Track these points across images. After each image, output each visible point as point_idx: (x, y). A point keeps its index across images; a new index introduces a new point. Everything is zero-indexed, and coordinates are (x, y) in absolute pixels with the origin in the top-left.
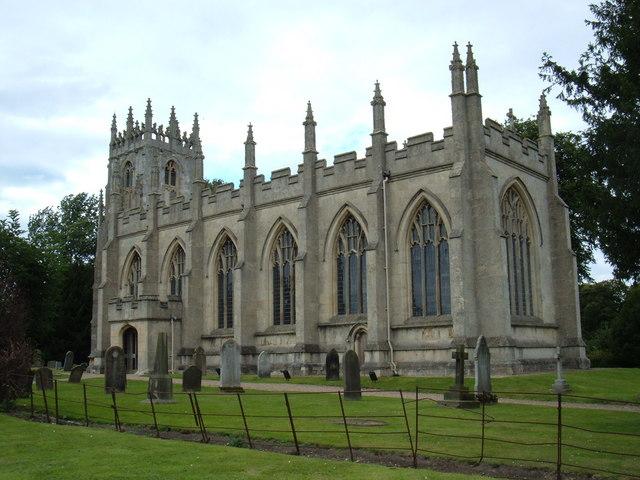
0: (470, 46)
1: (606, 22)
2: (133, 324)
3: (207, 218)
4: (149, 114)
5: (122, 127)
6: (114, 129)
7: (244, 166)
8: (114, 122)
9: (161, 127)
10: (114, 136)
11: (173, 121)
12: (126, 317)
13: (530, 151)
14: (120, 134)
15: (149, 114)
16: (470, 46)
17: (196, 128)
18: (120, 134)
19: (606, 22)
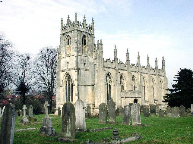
0: (163, 61)
1: (167, 103)
2: (137, 98)
3: (80, 85)
4: (76, 18)
5: (65, 23)
6: (62, 24)
7: (60, 34)
8: (62, 21)
9: (80, 23)
10: (62, 26)
11: (85, 21)
12: (136, 96)
13: (143, 68)
14: (65, 25)
15: (76, 18)
16: (163, 61)
17: (93, 23)
18: (65, 25)
19: (167, 103)
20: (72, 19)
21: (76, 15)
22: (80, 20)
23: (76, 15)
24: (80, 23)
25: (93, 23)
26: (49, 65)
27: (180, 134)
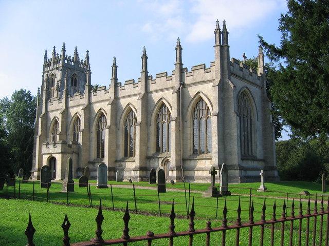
0: (224, 22)
2: (54, 155)
4: (64, 50)
5: (50, 56)
6: (46, 57)
10: (46, 61)
12: (51, 152)
14: (49, 60)
15: (64, 50)
16: (224, 22)
17: (88, 57)
18: (49, 60)
20: (59, 52)
21: (64, 46)
22: (70, 53)
23: (64, 46)
24: (70, 57)
25: (88, 57)
26: (218, 171)
27: (316, 112)
